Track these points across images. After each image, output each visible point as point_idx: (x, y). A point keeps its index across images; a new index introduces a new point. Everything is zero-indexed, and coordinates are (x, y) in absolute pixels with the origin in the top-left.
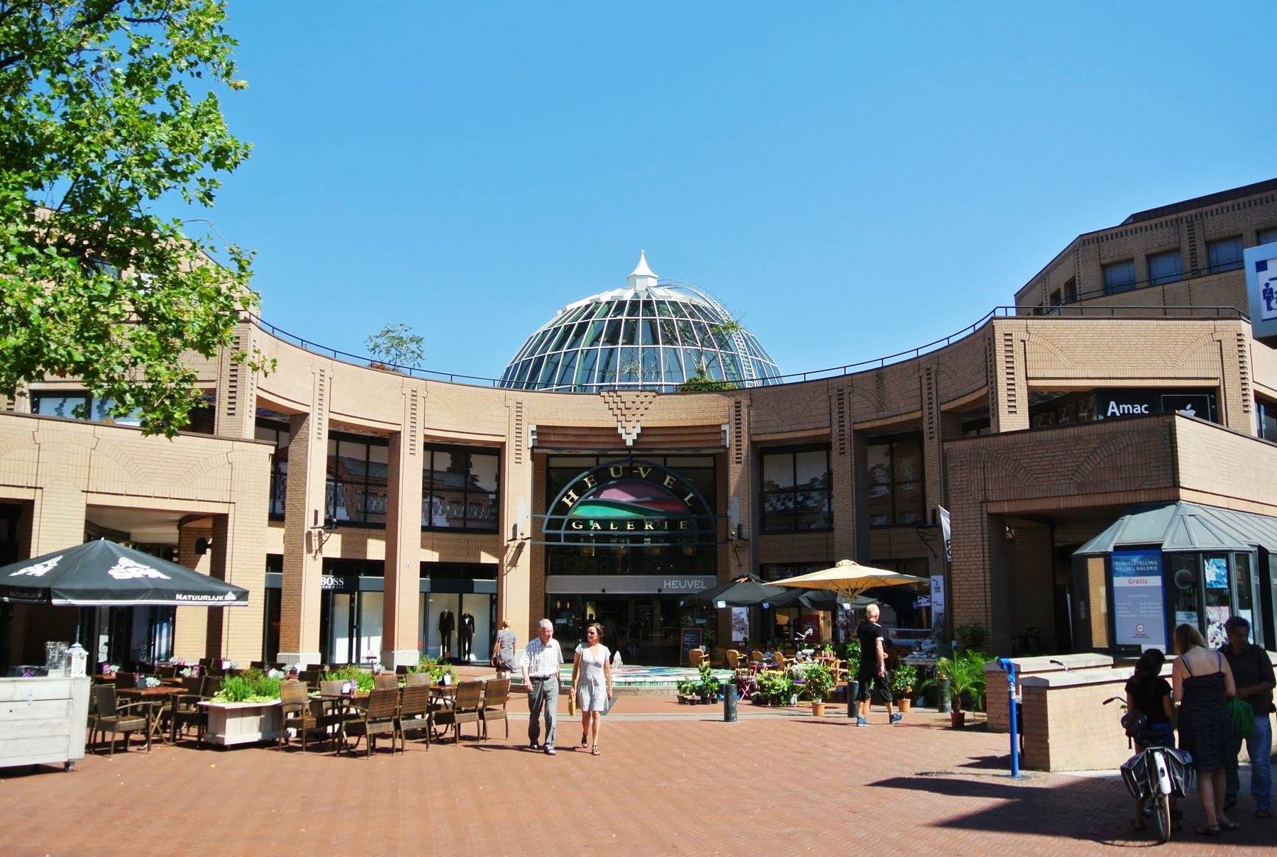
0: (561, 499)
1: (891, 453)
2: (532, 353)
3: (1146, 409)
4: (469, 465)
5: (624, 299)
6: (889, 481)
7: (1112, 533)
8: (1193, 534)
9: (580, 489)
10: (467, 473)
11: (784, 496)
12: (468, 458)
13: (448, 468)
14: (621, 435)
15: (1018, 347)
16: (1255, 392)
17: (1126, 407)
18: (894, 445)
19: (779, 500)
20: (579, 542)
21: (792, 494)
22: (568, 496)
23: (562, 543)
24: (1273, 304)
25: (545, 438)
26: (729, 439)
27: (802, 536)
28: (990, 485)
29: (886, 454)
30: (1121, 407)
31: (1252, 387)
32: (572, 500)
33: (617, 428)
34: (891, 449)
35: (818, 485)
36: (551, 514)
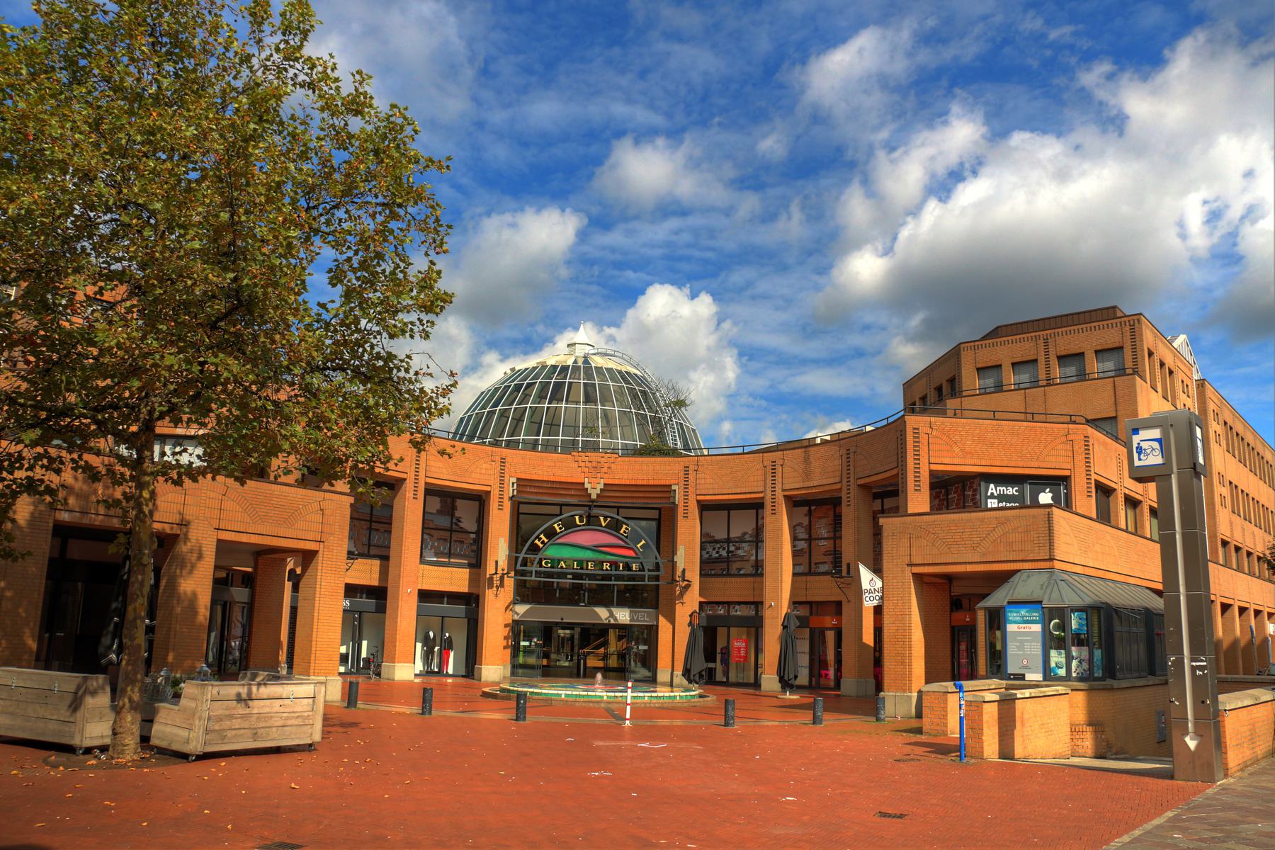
0: (534, 541)
1: (810, 513)
2: (484, 407)
3: (1016, 491)
4: (454, 508)
5: (568, 364)
6: (807, 537)
7: (1005, 593)
8: (1063, 592)
9: (551, 534)
10: (453, 515)
11: (719, 546)
12: (453, 503)
13: (438, 510)
14: (587, 489)
15: (924, 439)
16: (1095, 480)
17: (1002, 489)
18: (813, 508)
19: (714, 549)
20: (611, 581)
21: (726, 545)
22: (540, 539)
23: (533, 578)
24: (1142, 456)
25: (524, 489)
26: (679, 498)
27: (733, 579)
28: (914, 553)
29: (806, 515)
30: (998, 488)
31: (1094, 477)
32: (543, 542)
33: (584, 484)
34: (810, 511)
35: (747, 538)
36: (526, 553)
